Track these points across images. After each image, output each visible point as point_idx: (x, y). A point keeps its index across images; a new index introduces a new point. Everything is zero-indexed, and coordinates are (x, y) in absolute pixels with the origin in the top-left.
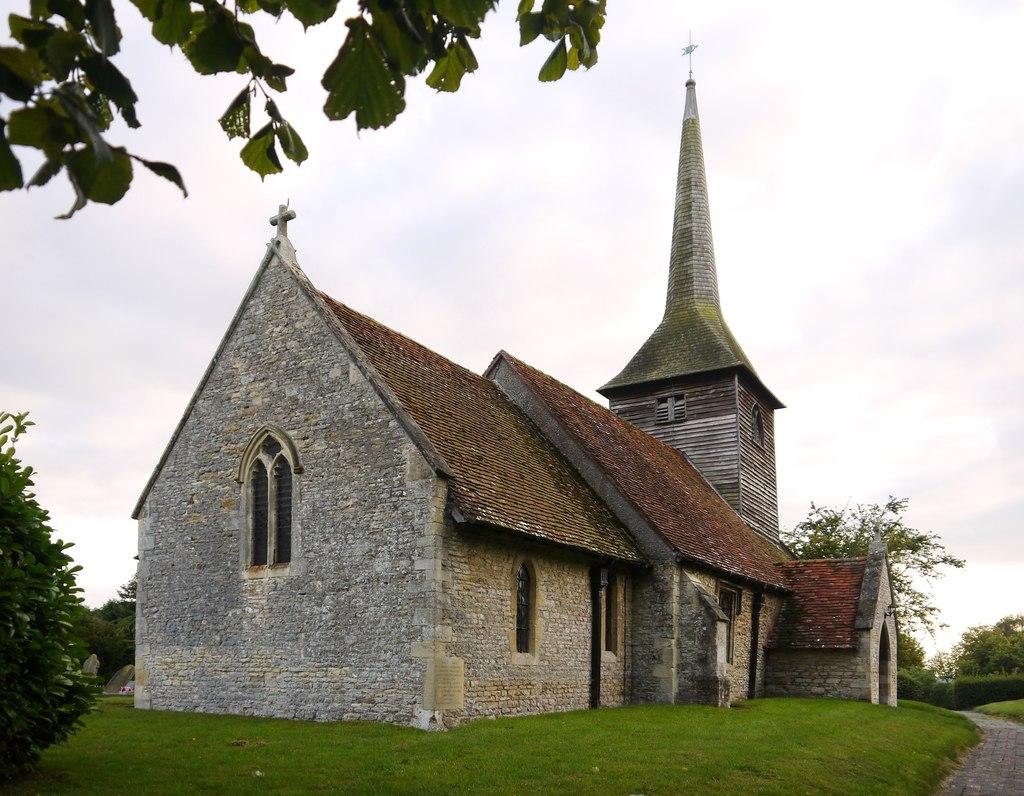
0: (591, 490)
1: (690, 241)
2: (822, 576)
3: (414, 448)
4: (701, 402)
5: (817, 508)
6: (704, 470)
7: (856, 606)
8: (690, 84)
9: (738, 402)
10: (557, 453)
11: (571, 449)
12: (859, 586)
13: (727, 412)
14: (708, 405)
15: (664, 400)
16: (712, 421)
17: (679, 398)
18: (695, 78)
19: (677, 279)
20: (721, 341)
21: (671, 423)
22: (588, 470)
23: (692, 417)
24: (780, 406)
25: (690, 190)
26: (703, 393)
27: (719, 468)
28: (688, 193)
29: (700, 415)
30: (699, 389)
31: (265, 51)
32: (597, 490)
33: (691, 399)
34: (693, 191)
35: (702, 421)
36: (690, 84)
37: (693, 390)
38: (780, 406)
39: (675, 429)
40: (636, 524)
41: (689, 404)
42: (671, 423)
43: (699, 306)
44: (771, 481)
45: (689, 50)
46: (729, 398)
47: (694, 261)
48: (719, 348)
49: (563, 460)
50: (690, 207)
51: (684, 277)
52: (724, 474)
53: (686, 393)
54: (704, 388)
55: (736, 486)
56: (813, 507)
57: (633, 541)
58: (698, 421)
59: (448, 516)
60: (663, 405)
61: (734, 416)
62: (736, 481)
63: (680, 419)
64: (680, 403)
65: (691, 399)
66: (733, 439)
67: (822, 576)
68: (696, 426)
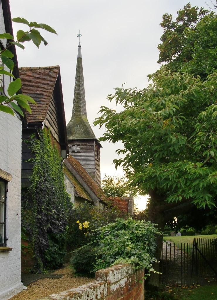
0: (79, 182)
1: (80, 96)
2: (119, 202)
3: (69, 181)
4: (85, 148)
5: (106, 176)
6: (85, 168)
7: (128, 210)
8: (80, 46)
9: (95, 149)
10: (70, 172)
11: (74, 172)
12: (128, 205)
13: (91, 151)
14: (87, 149)
15: (74, 145)
16: (88, 154)
17: (78, 145)
18: (81, 45)
19: (76, 107)
20: (90, 130)
21: (76, 153)
22: (78, 177)
23: (82, 152)
24: (102, 147)
25: (80, 80)
26: (85, 145)
27: (90, 168)
28: (79, 81)
29: (84, 151)
30: (84, 144)
31: (118, 160)
32: (80, 182)
33: (82, 146)
34: (81, 81)
35: (85, 153)
36: (80, 46)
37: (82, 144)
38: (102, 147)
39: (77, 155)
40: (90, 192)
41: (82, 148)
42: (76, 153)
43: (83, 117)
44: (99, 171)
45: (79, 36)
46: (92, 147)
47: (81, 102)
48: (89, 132)
49: (72, 174)
50: (80, 86)
51: (78, 107)
52: (91, 170)
53: (81, 144)
54: (85, 144)
55: (94, 173)
56: (106, 175)
57: (89, 195)
58: (83, 153)
59: (75, 196)
60: (74, 147)
61: (94, 153)
62: (94, 172)
63: (79, 152)
64: (79, 147)
65: (82, 146)
66: (93, 160)
67: (119, 202)
68: (83, 155)
